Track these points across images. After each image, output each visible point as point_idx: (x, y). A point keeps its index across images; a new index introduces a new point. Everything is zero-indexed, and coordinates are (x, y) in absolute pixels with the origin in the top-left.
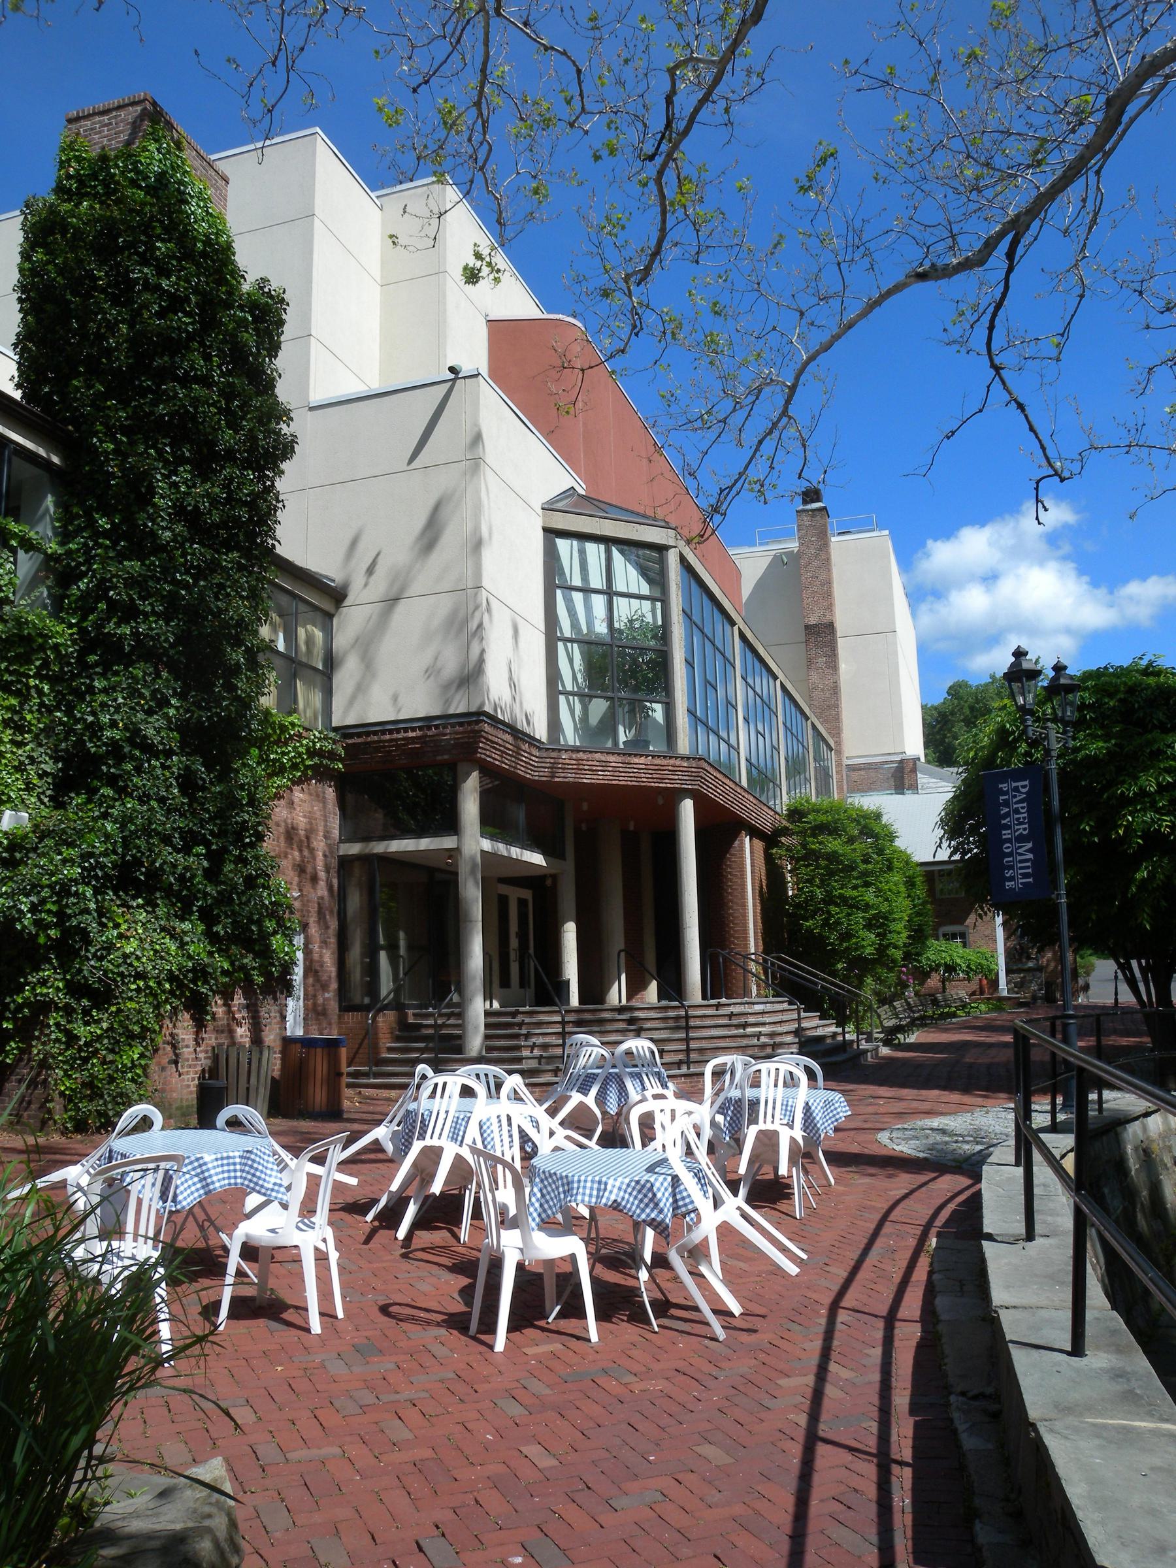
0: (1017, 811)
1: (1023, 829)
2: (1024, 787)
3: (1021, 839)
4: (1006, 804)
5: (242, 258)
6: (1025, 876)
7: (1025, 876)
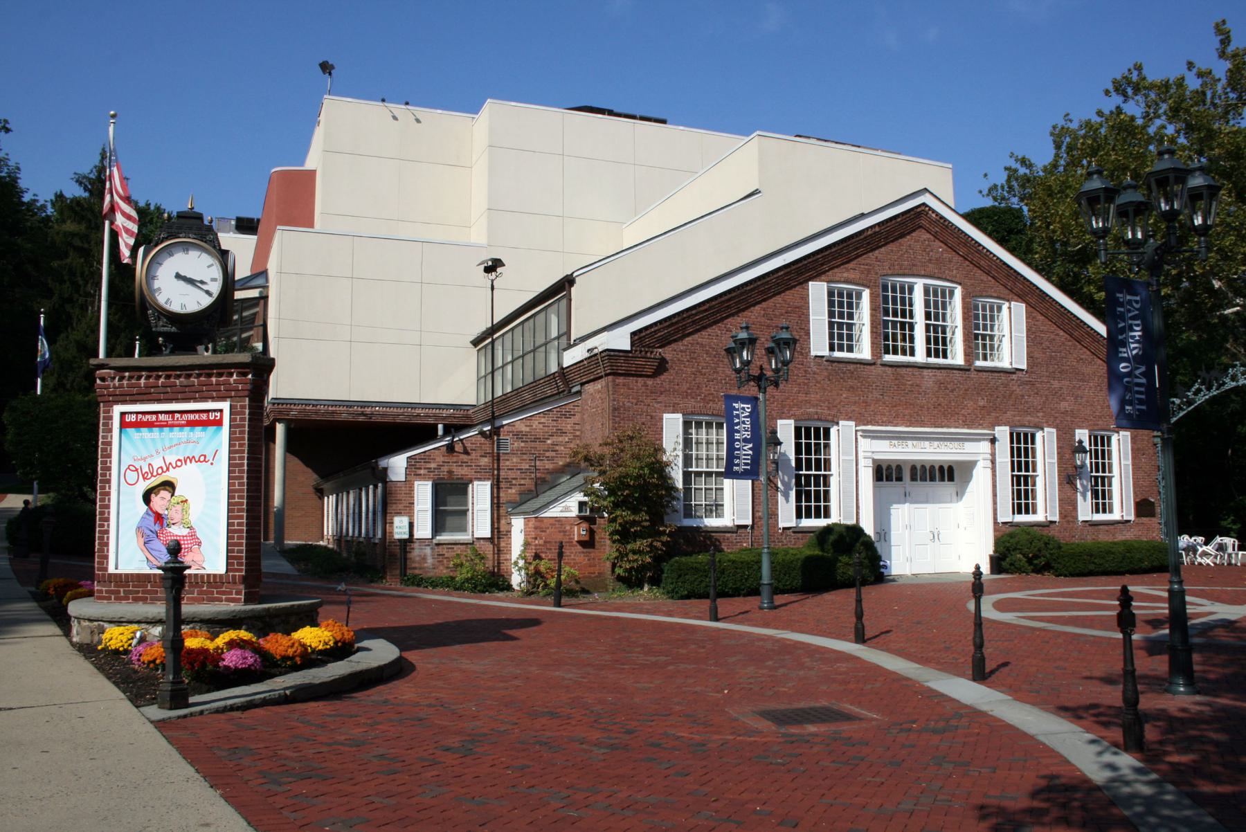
0: (744, 422)
1: (747, 435)
2: (1137, 302)
3: (746, 440)
4: (738, 416)
5: (22, 184)
6: (746, 464)
7: (746, 464)
